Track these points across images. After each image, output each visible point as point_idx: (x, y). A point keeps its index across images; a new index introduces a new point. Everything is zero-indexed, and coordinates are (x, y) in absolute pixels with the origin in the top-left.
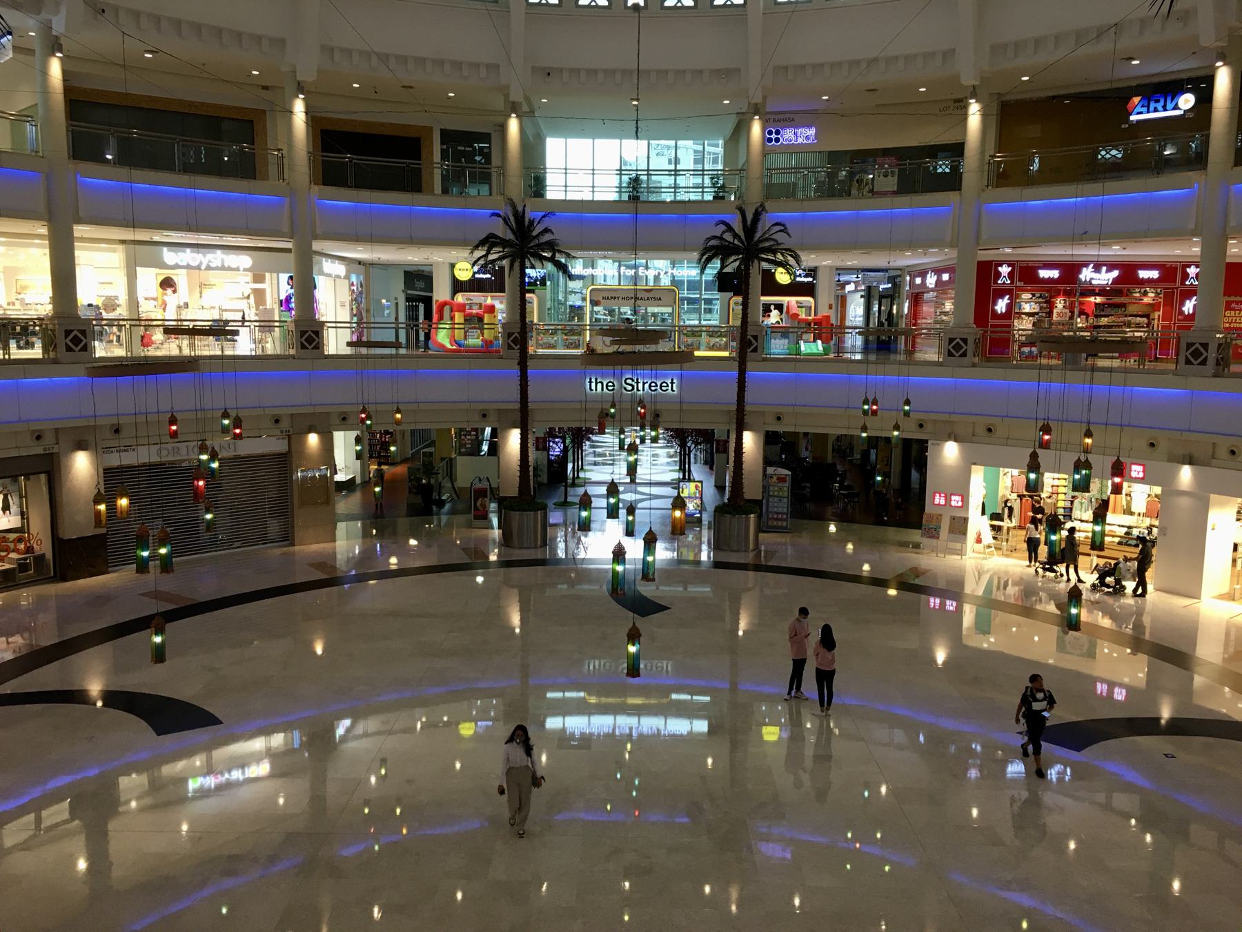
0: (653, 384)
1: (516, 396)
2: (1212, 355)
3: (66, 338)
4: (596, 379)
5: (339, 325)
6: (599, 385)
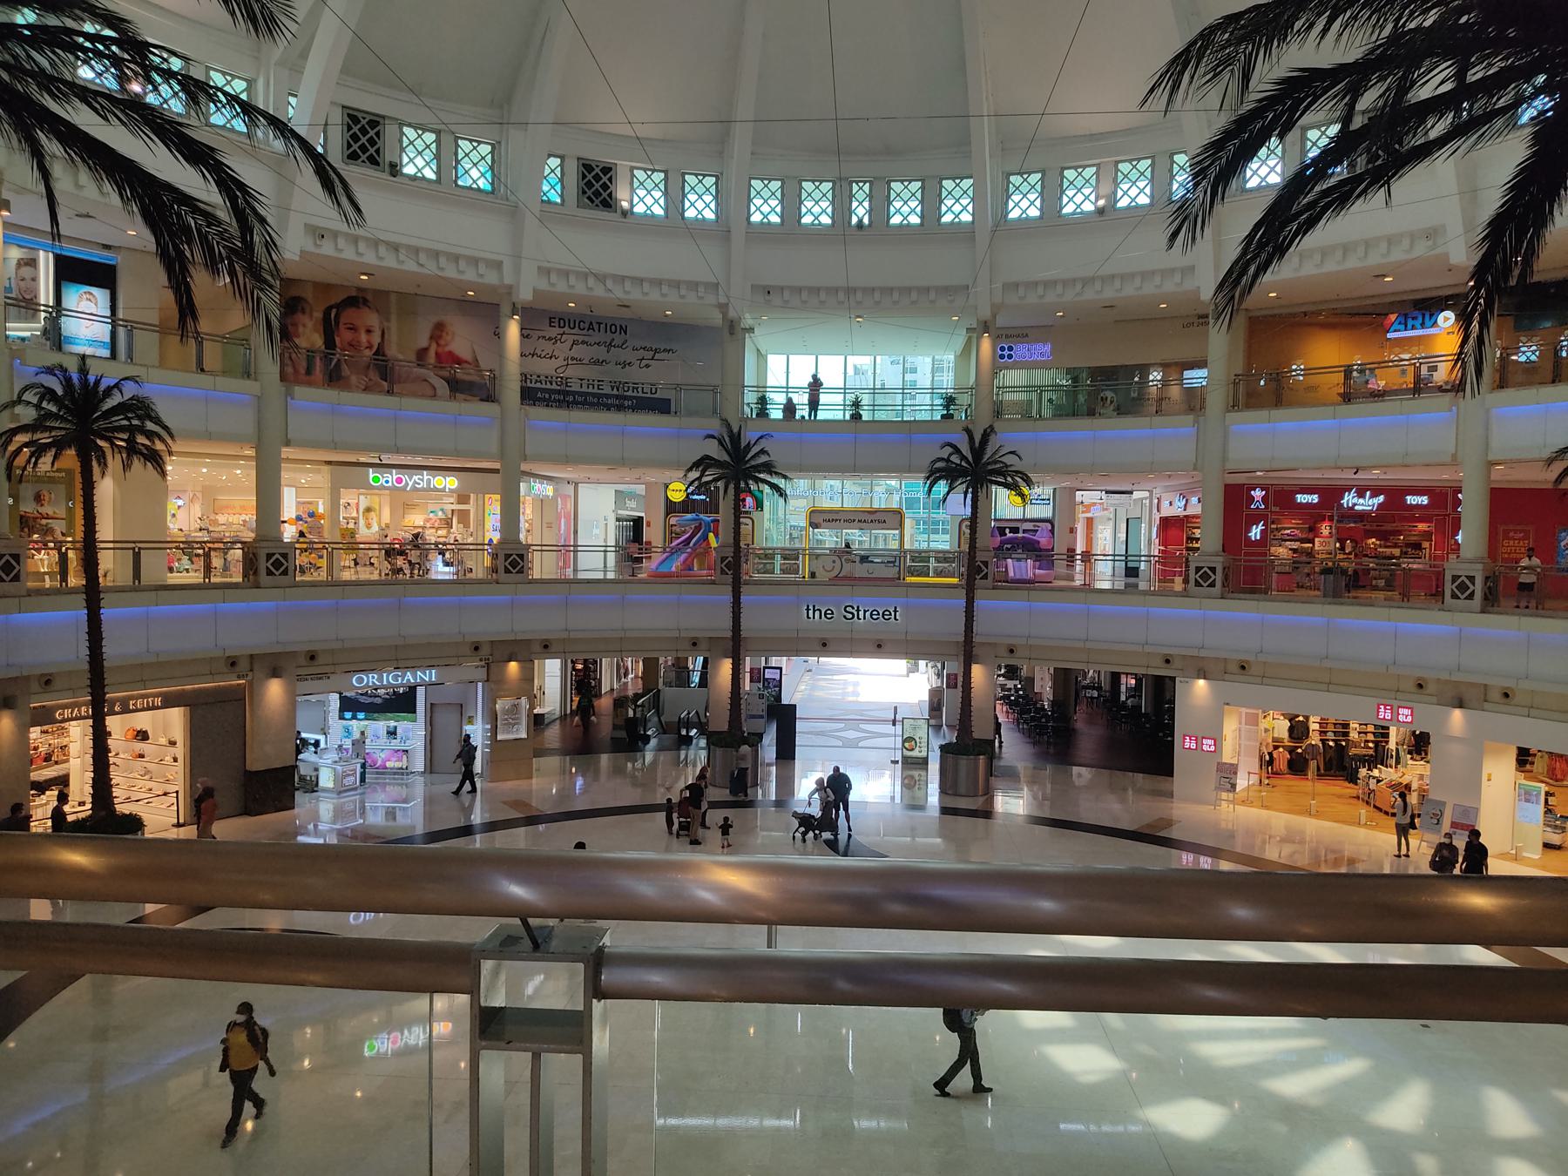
1: (728, 623)
4: (814, 606)
6: (817, 613)
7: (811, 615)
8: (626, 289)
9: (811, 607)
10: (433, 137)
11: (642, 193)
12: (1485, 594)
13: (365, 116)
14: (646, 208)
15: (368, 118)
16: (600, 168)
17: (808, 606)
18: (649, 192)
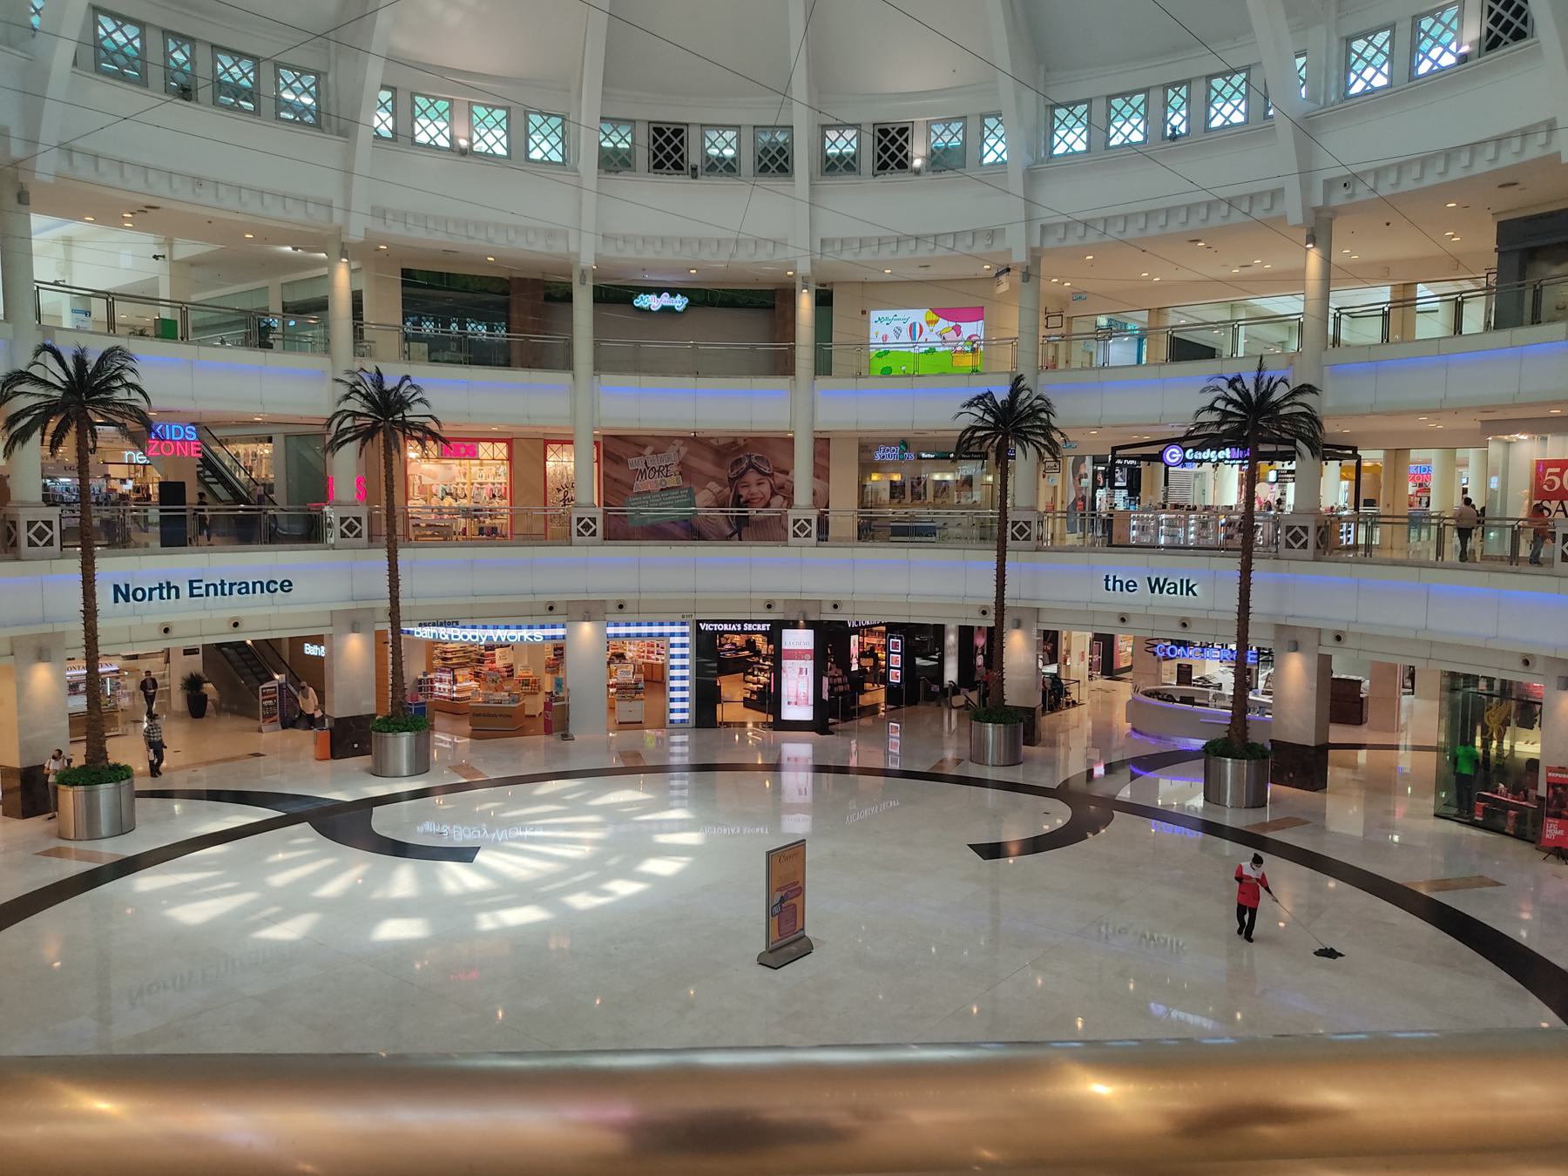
0: (1131, 584)
1: (992, 591)
2: (1311, 538)
3: (37, 545)
4: (1115, 577)
5: (1397, 520)
6: (1118, 584)
7: (1110, 586)
8: (510, 238)
9: (1111, 578)
10: (504, 113)
11: (424, 122)
12: (15, 528)
13: (668, 126)
14: (543, 154)
15: (673, 128)
16: (671, 130)
17: (1107, 576)
18: (432, 121)
